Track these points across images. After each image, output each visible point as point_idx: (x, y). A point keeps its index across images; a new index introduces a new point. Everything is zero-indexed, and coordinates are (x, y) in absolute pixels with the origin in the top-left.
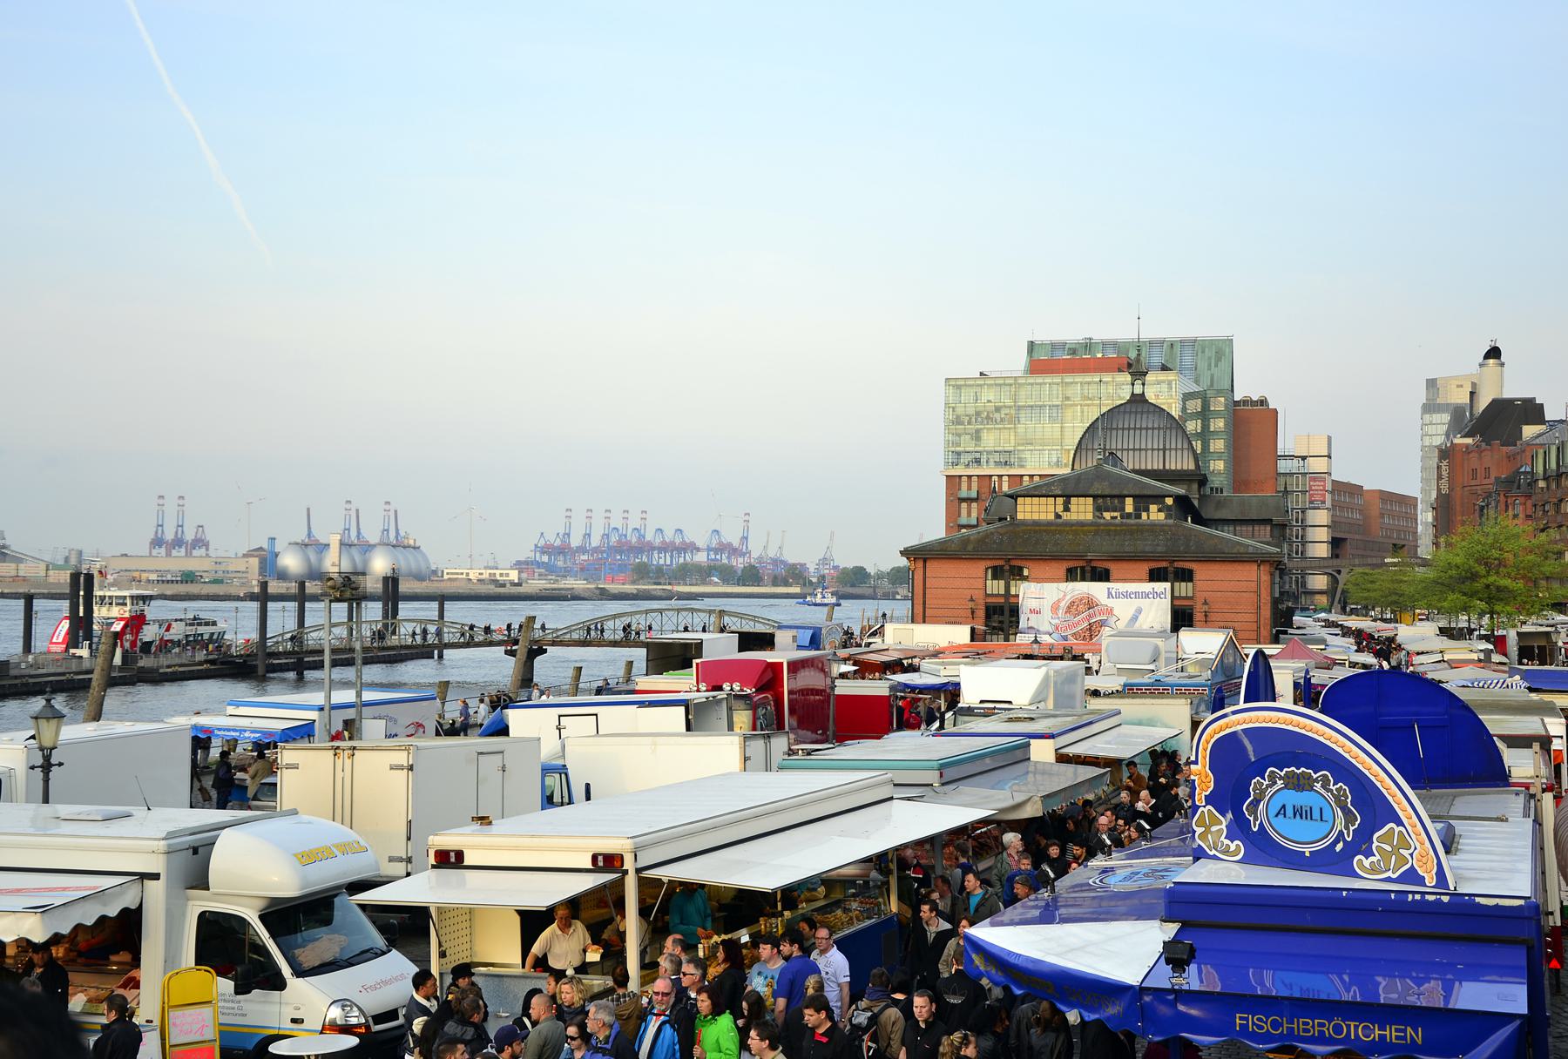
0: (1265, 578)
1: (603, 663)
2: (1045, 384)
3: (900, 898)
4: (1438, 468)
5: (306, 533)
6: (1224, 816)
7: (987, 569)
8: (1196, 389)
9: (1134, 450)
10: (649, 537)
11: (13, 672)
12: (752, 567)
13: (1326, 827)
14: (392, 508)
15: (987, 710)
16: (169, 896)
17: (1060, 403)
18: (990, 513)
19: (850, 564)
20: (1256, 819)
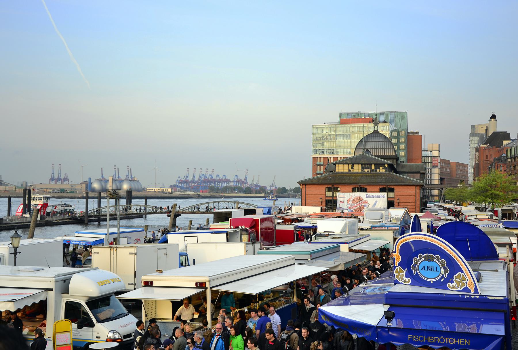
0: (418, 191)
1: (199, 219)
2: (345, 127)
4: (475, 155)
5: (101, 176)
6: (404, 270)
7: (326, 188)
8: (395, 128)
9: (375, 149)
10: (214, 177)
11: (4, 222)
12: (248, 187)
13: (438, 273)
15: (326, 235)
16: (56, 296)
17: (350, 133)
18: (327, 170)
20: (415, 271)
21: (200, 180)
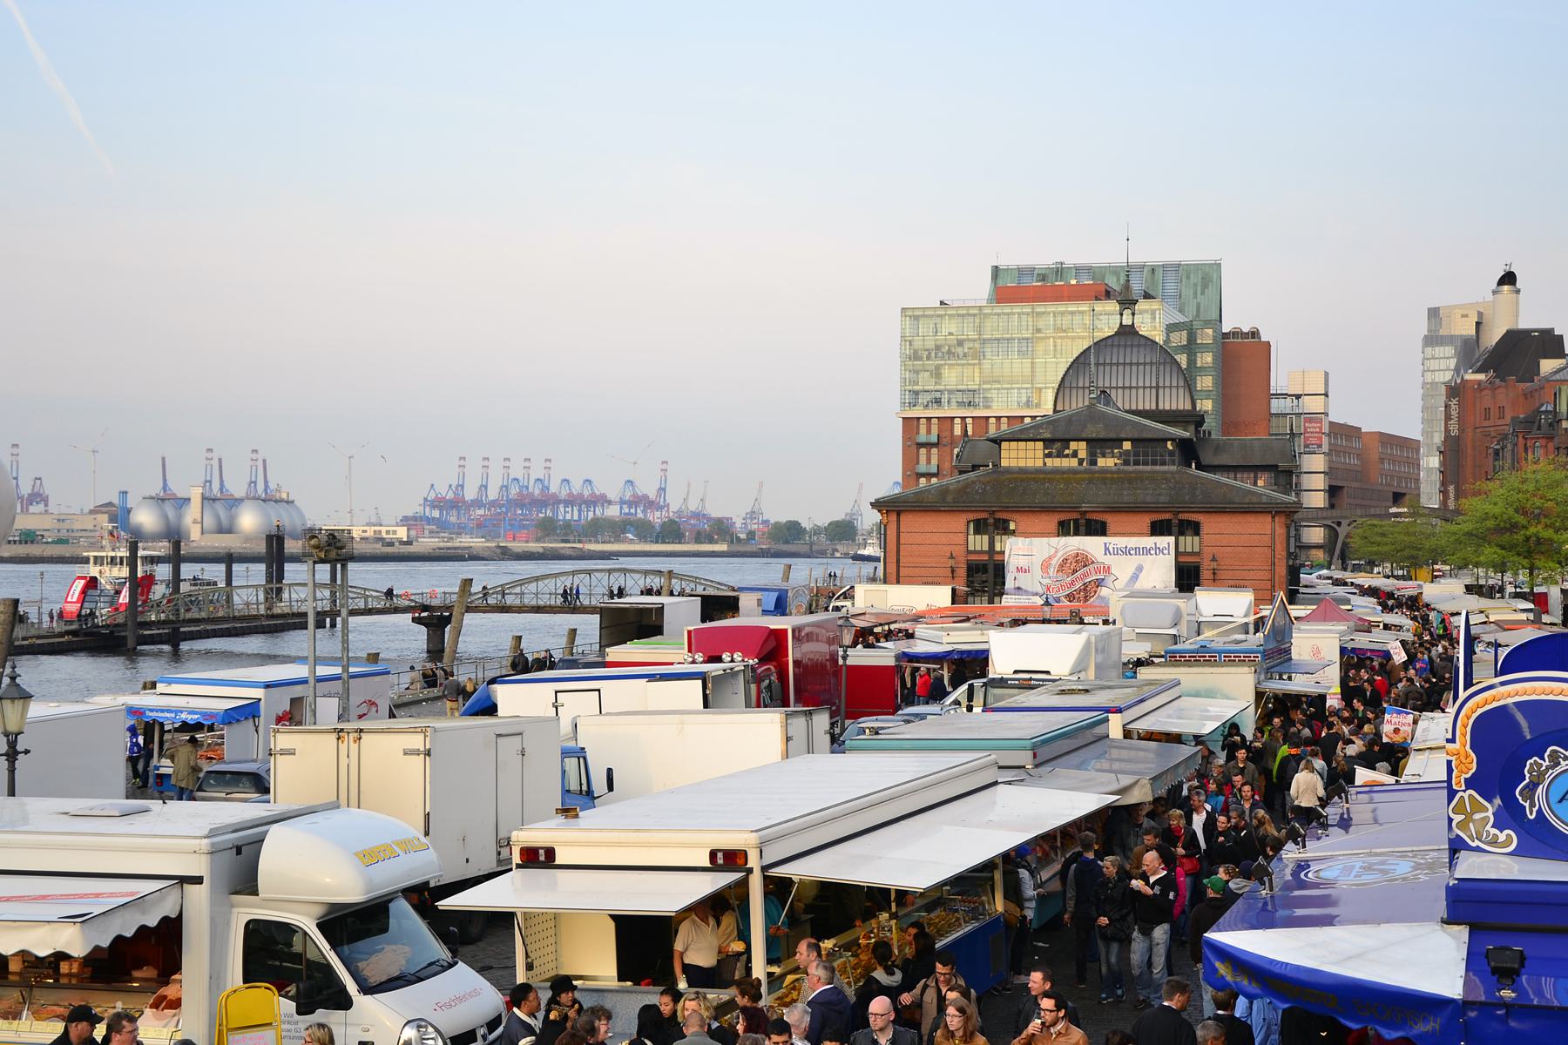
0: (1280, 531)
2: (1013, 314)
3: (1006, 897)
4: (1446, 407)
5: (162, 485)
6: (1489, 800)
7: (969, 522)
8: (1181, 318)
9: (1123, 388)
10: (553, 489)
12: (672, 522)
14: (260, 456)
15: (1027, 681)
16: (213, 903)
17: (1030, 336)
18: (963, 459)
19: (783, 519)
20: (1532, 805)
21: (505, 498)
